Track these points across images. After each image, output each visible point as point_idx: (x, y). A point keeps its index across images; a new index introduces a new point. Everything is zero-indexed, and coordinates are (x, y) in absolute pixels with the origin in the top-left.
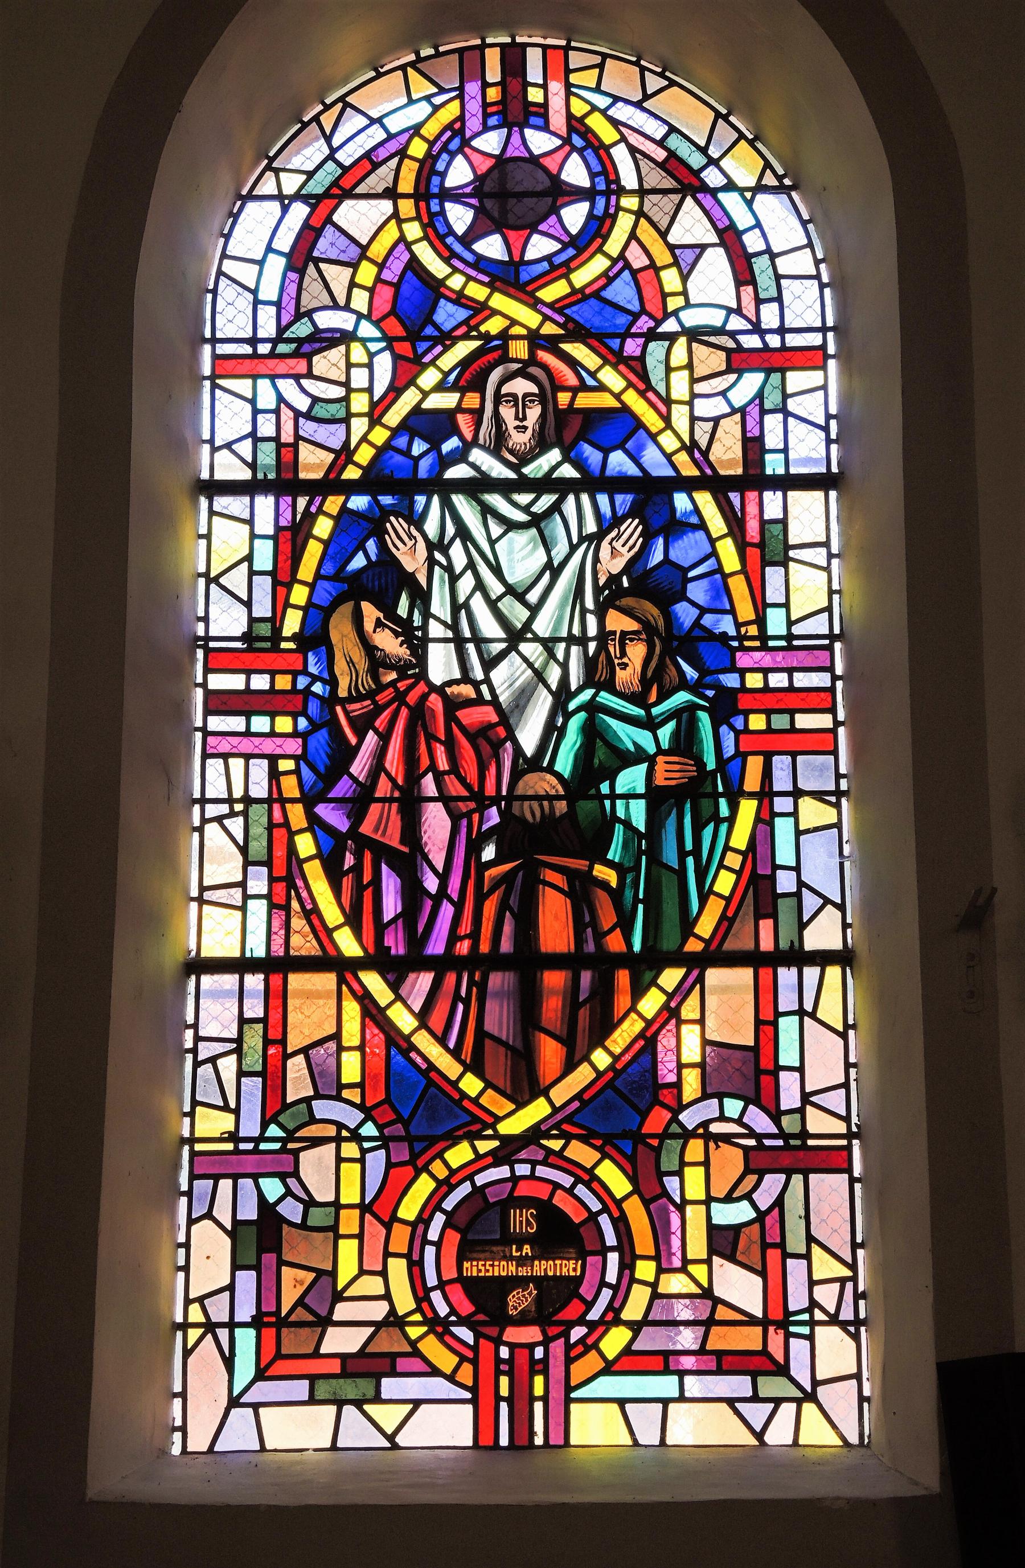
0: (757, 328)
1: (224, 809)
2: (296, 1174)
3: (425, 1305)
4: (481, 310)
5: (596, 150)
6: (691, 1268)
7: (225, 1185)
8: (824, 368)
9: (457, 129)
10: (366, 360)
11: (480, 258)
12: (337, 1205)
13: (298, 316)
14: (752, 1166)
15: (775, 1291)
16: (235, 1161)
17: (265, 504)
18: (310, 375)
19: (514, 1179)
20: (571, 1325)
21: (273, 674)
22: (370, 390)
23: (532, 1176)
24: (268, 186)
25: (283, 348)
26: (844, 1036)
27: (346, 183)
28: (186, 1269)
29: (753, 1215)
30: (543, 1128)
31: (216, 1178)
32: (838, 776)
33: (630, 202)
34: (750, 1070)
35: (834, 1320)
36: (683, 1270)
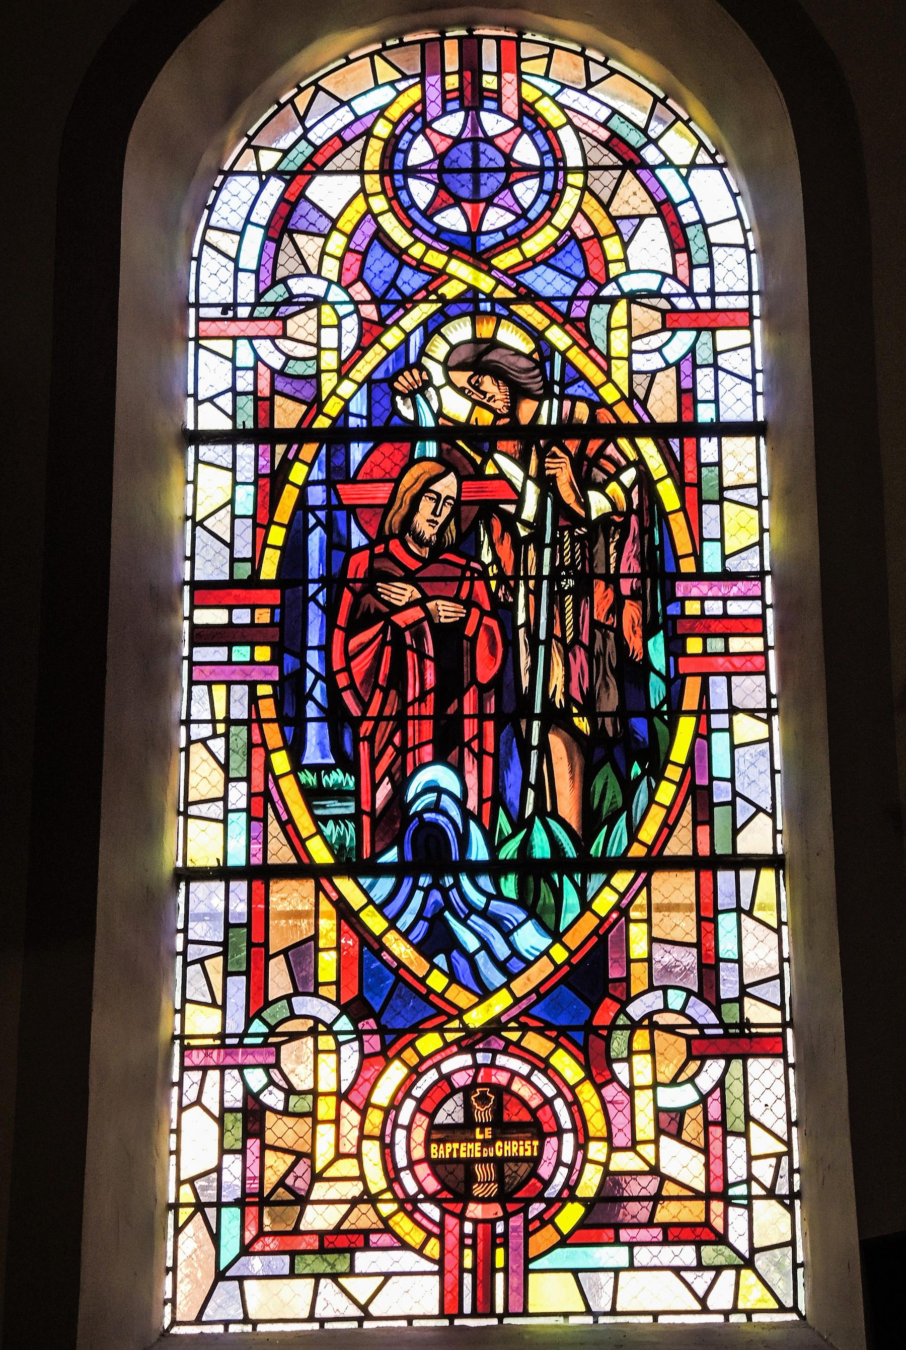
2: (277, 1065)
3: (396, 1187)
4: (440, 275)
7: (213, 1076)
8: (750, 328)
11: (441, 229)
12: (314, 1093)
13: (275, 283)
14: (694, 1053)
16: (228, 1049)
17: (246, 451)
18: (284, 336)
19: (476, 1066)
20: (529, 1202)
21: (253, 608)
22: (339, 349)
25: (260, 311)
26: (778, 931)
27: (319, 160)
28: (177, 1153)
30: (504, 1019)
32: (770, 696)
33: (576, 179)
35: (770, 1194)
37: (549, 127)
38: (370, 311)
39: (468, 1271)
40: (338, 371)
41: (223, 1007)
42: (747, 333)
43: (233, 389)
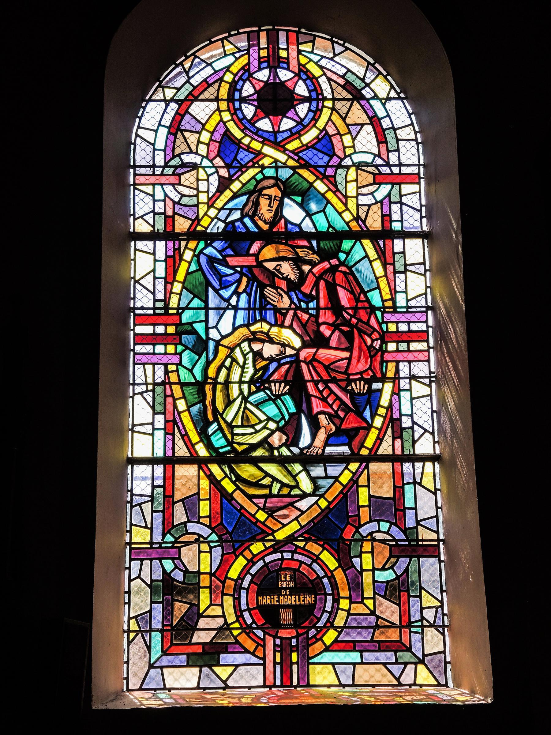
0: (388, 164)
1: (144, 388)
2: (179, 558)
3: (241, 619)
5: (310, 79)
6: (365, 601)
7: (147, 563)
8: (419, 183)
9: (246, 70)
10: (206, 178)
11: (259, 129)
12: (199, 573)
13: (174, 157)
15: (405, 612)
16: (151, 552)
17: (160, 244)
18: (180, 184)
20: (310, 628)
21: (166, 325)
22: (208, 192)
23: (292, 559)
24: (159, 95)
26: (435, 494)
27: (196, 93)
29: (394, 576)
31: (142, 560)
33: (329, 104)
34: (392, 508)
36: (362, 602)
37: (314, 77)
38: (224, 172)
39: (278, 663)
40: (207, 203)
41: (151, 529)
42: (418, 186)
43: (153, 211)
